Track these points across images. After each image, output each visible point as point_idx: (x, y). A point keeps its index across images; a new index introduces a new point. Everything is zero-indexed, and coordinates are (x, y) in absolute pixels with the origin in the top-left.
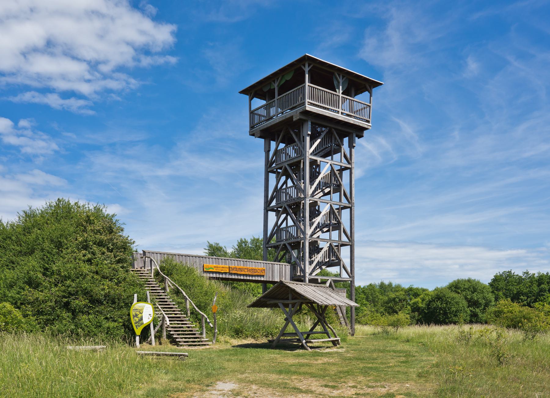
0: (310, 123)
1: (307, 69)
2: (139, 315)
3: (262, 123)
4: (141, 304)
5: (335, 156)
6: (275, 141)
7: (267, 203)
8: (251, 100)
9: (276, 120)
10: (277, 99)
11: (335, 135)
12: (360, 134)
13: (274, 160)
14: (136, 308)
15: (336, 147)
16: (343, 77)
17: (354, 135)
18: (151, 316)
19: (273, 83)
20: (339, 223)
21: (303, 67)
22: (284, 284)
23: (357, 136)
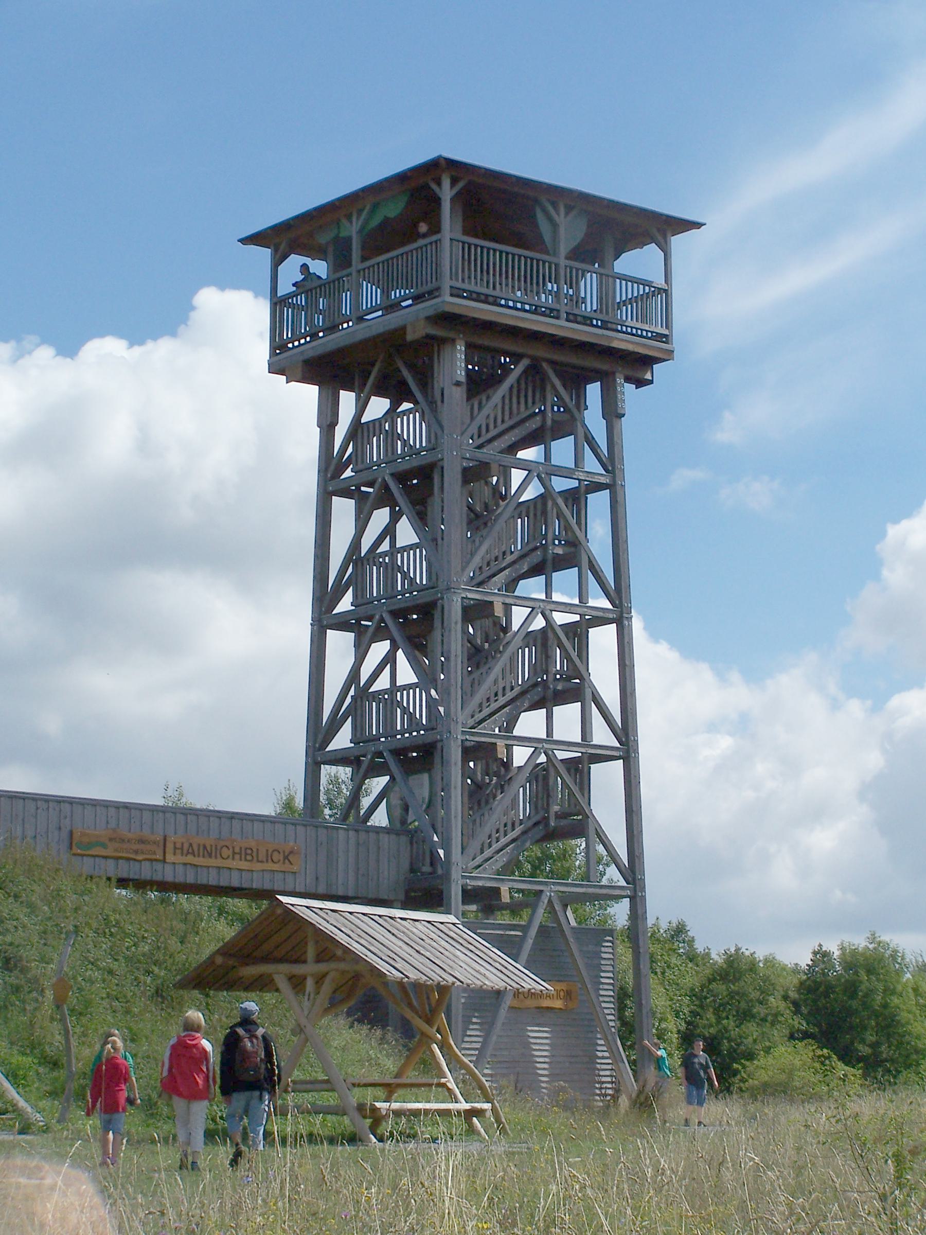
0: (461, 347)
1: (446, 192)
5: (555, 445)
10: (359, 271)
17: (620, 380)
19: (344, 221)
21: (434, 186)
23: (628, 380)
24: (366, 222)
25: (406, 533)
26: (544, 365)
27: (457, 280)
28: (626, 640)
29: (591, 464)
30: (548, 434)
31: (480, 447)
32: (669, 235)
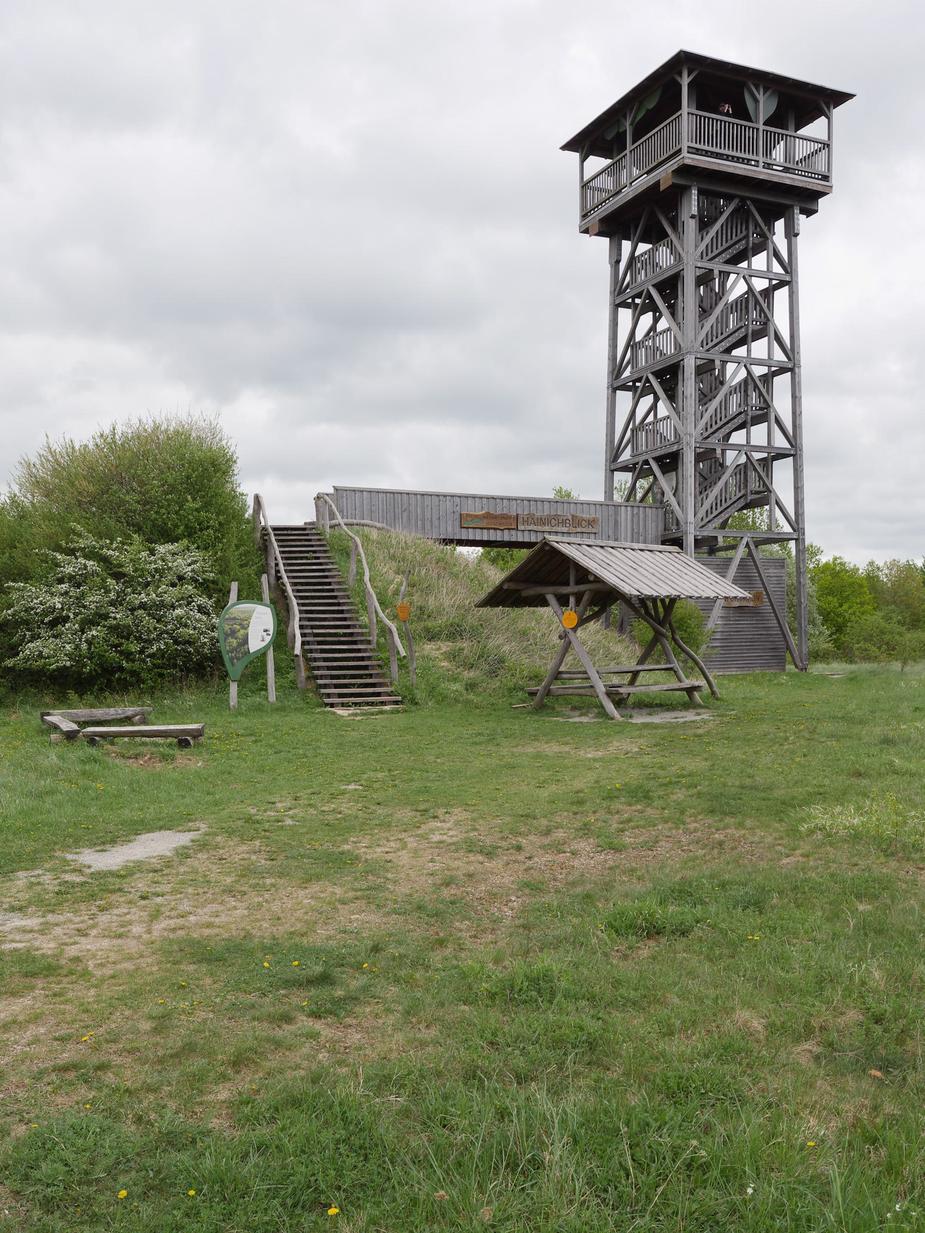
0: (695, 192)
4: (245, 606)
5: (754, 429)
6: (630, 240)
8: (583, 160)
9: (628, 193)
14: (232, 616)
15: (758, 240)
17: (797, 211)
20: (767, 406)
21: (678, 79)
22: (259, 514)
23: (802, 212)
24: (635, 117)
25: (663, 409)
26: (749, 202)
27: (692, 142)
28: (797, 381)
29: (779, 355)
30: (750, 253)
31: (708, 350)
32: (832, 107)
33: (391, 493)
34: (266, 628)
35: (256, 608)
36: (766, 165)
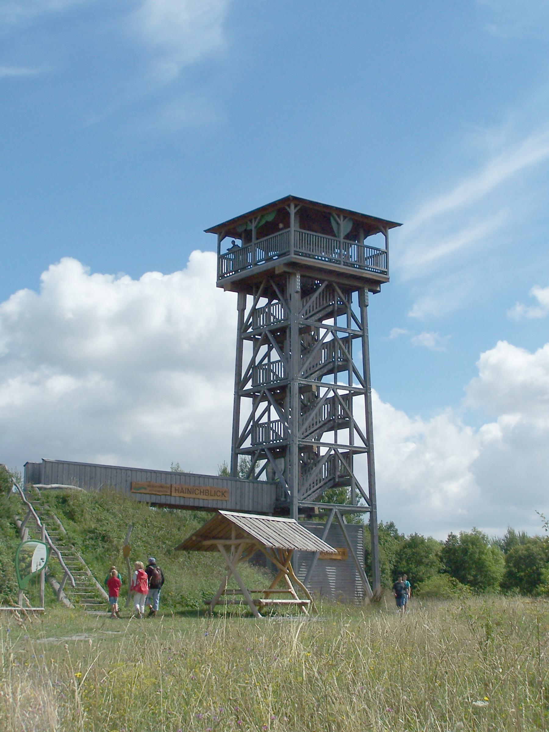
0: (298, 277)
1: (293, 211)
2: (27, 558)
3: (231, 274)
7: (240, 384)
11: (337, 291)
12: (374, 288)
13: (251, 323)
16: (345, 218)
17: (366, 291)
18: (43, 562)
19: (249, 222)
21: (287, 208)
23: (370, 291)
24: (259, 223)
26: (334, 284)
33: (83, 465)
34: (42, 557)
35: (37, 545)
36: (345, 263)
